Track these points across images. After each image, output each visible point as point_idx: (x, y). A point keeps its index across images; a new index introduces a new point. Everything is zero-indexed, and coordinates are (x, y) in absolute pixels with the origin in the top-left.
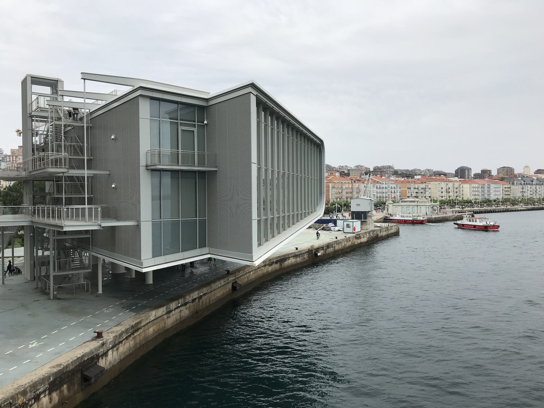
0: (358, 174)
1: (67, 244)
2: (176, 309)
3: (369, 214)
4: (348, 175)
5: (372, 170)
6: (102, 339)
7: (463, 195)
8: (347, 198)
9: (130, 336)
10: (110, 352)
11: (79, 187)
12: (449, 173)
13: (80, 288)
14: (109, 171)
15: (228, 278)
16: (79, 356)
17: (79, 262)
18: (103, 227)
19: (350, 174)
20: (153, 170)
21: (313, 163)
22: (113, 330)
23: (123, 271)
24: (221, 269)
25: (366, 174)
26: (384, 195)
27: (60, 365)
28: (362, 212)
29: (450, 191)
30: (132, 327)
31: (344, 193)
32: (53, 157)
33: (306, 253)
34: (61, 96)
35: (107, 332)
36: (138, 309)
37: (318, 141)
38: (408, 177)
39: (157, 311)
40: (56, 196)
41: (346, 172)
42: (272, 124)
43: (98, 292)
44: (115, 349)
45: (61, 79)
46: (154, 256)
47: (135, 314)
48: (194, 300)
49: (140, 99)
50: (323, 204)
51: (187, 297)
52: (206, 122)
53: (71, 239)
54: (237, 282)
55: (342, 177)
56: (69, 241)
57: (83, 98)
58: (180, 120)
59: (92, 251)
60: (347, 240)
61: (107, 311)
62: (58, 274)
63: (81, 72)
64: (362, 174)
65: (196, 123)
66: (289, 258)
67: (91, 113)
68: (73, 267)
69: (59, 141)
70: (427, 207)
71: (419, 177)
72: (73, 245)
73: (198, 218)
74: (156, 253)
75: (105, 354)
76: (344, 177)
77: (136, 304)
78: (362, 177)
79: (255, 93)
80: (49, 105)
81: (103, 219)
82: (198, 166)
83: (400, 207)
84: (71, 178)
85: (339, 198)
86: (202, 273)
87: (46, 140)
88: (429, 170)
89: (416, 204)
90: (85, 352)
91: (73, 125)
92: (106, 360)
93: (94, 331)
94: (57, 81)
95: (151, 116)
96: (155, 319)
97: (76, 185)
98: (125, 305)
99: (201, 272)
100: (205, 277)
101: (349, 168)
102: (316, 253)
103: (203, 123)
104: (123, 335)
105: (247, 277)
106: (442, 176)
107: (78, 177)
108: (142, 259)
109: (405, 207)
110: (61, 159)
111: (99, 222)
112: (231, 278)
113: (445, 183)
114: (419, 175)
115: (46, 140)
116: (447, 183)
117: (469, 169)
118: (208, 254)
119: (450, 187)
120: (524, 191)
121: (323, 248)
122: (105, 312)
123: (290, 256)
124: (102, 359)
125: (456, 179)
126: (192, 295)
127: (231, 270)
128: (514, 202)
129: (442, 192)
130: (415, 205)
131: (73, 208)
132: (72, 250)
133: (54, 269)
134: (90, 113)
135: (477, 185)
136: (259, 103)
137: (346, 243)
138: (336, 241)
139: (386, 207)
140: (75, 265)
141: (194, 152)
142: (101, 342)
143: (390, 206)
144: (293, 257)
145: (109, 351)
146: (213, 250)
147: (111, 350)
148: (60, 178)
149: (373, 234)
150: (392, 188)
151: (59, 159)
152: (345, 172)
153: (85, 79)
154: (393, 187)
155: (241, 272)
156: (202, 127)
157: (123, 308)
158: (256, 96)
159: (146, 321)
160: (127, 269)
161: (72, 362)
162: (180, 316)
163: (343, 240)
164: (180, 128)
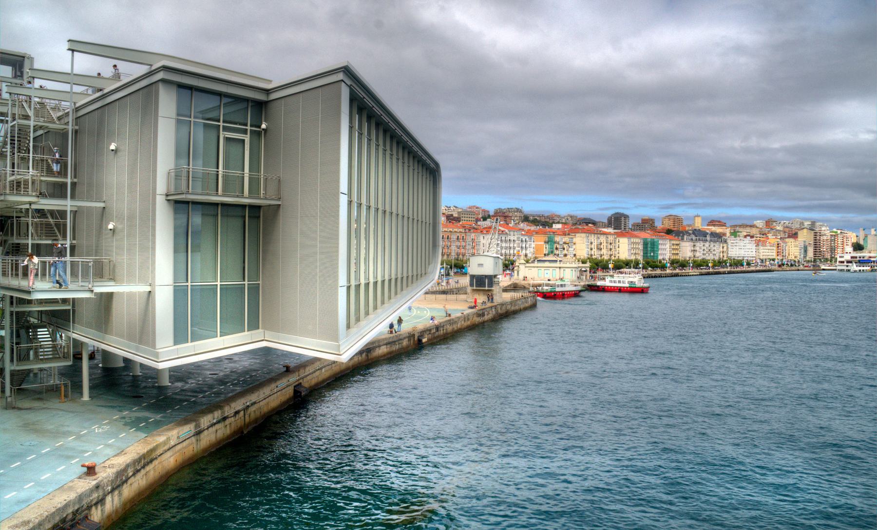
0: (473, 219)
1: (32, 320)
2: (210, 427)
3: (496, 280)
4: (458, 220)
5: (492, 213)
6: (94, 477)
7: (618, 253)
8: (458, 254)
9: (138, 471)
10: (109, 499)
11: (53, 228)
12: (599, 222)
13: (54, 391)
14: (104, 202)
15: (288, 378)
16: (59, 506)
17: (51, 349)
18: (96, 294)
19: (462, 219)
20: (177, 202)
21: (424, 198)
22: (112, 462)
23: (121, 364)
24: (276, 363)
25: (485, 219)
26: (512, 252)
27: (29, 522)
28: (486, 276)
29: (602, 247)
30: (144, 456)
31: (453, 248)
32: (13, 178)
33: (405, 338)
34: (9, 94)
35: (103, 465)
36: (151, 427)
37: (432, 165)
38: (544, 224)
39: (181, 428)
40: (17, 241)
41: (456, 215)
42: (369, 134)
43: (82, 397)
44: (116, 492)
45: (30, 55)
46: (176, 342)
47: (146, 435)
48: (237, 413)
49: (161, 87)
50: (436, 263)
51: (226, 409)
52: (264, 126)
53: (39, 311)
54: (302, 384)
55: (450, 222)
56: (36, 315)
57: (69, 83)
58: (224, 122)
59: (73, 332)
60: (465, 318)
61: (100, 430)
62: (18, 368)
63: (68, 39)
64: (477, 220)
65: (249, 128)
66: (379, 346)
67: (77, 109)
68: (42, 357)
69: (23, 152)
70: (574, 269)
71: (559, 226)
72: (42, 321)
73: (246, 283)
74: (180, 337)
75: (101, 501)
76: (453, 223)
77: (146, 420)
78: (479, 223)
79: (349, 82)
80: (10, 94)
81: (84, 280)
82: (250, 197)
83: (536, 268)
84: (41, 213)
85: (447, 255)
86: (245, 369)
87: (3, 150)
88: (571, 217)
89: (558, 264)
90: (68, 499)
91: (47, 127)
92: (102, 510)
93: (81, 463)
94: (24, 57)
95: (178, 115)
96: (178, 444)
97: (48, 225)
98: (128, 421)
99: (246, 367)
100: (251, 376)
101: (460, 210)
102: (420, 338)
103: (259, 127)
104: (129, 469)
105: (317, 377)
106: (590, 225)
107: (52, 213)
108: (158, 345)
109: (543, 269)
110: (26, 181)
111: (90, 286)
112: (293, 379)
113: (596, 236)
114: (558, 223)
115: (3, 150)
116: (599, 236)
117: (626, 217)
118: (263, 340)
119: (602, 241)
120: (695, 249)
121: (430, 330)
122: (96, 431)
123: (381, 344)
124: (97, 508)
125: (610, 230)
126: (233, 405)
127: (292, 365)
128: (683, 265)
129: (591, 249)
130: (556, 267)
131: (46, 262)
132: (31, 330)
133: (12, 360)
134: (76, 108)
135: (637, 240)
136: (353, 98)
137: (463, 322)
138: (449, 321)
139: (515, 268)
140: (45, 353)
141: (244, 174)
142: (94, 483)
143: (522, 267)
144: (386, 344)
145: (107, 497)
146: (269, 335)
147: (110, 495)
148: (22, 212)
149: (501, 309)
150: (522, 241)
151: (17, 183)
152: (454, 215)
153: (73, 51)
154: (524, 239)
155: (307, 369)
156: (257, 135)
157: (126, 424)
158: (350, 87)
159: (164, 446)
160: (126, 360)
161: (47, 516)
162: (216, 437)
163: (459, 318)
164: (223, 135)
